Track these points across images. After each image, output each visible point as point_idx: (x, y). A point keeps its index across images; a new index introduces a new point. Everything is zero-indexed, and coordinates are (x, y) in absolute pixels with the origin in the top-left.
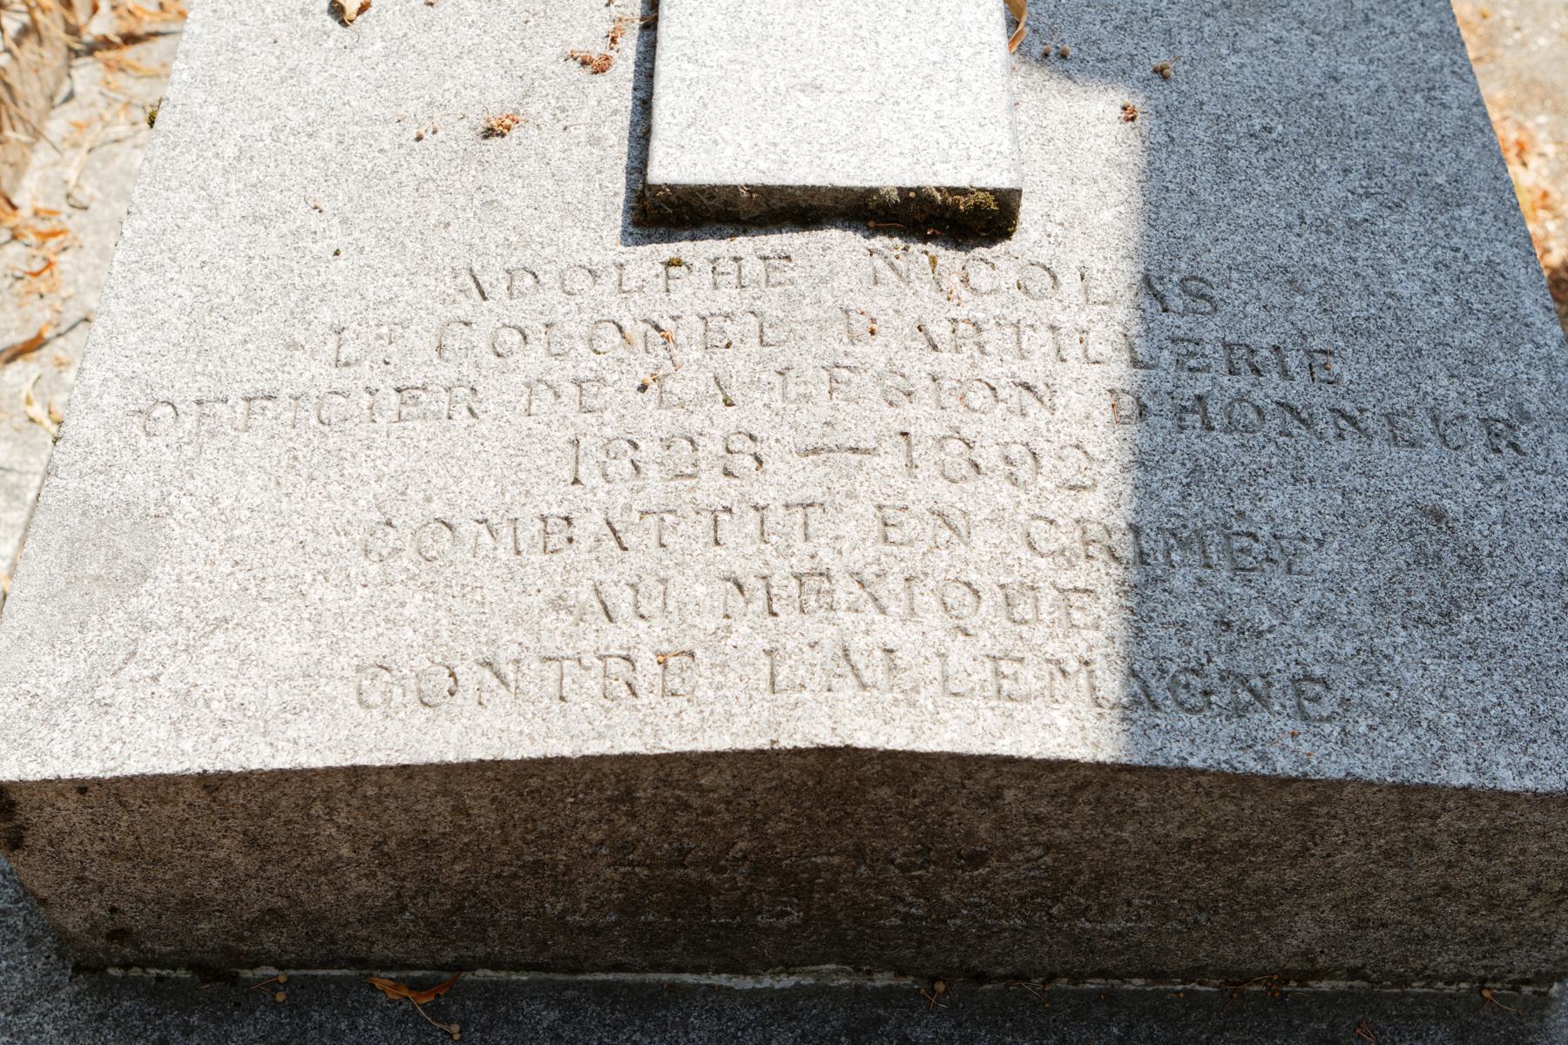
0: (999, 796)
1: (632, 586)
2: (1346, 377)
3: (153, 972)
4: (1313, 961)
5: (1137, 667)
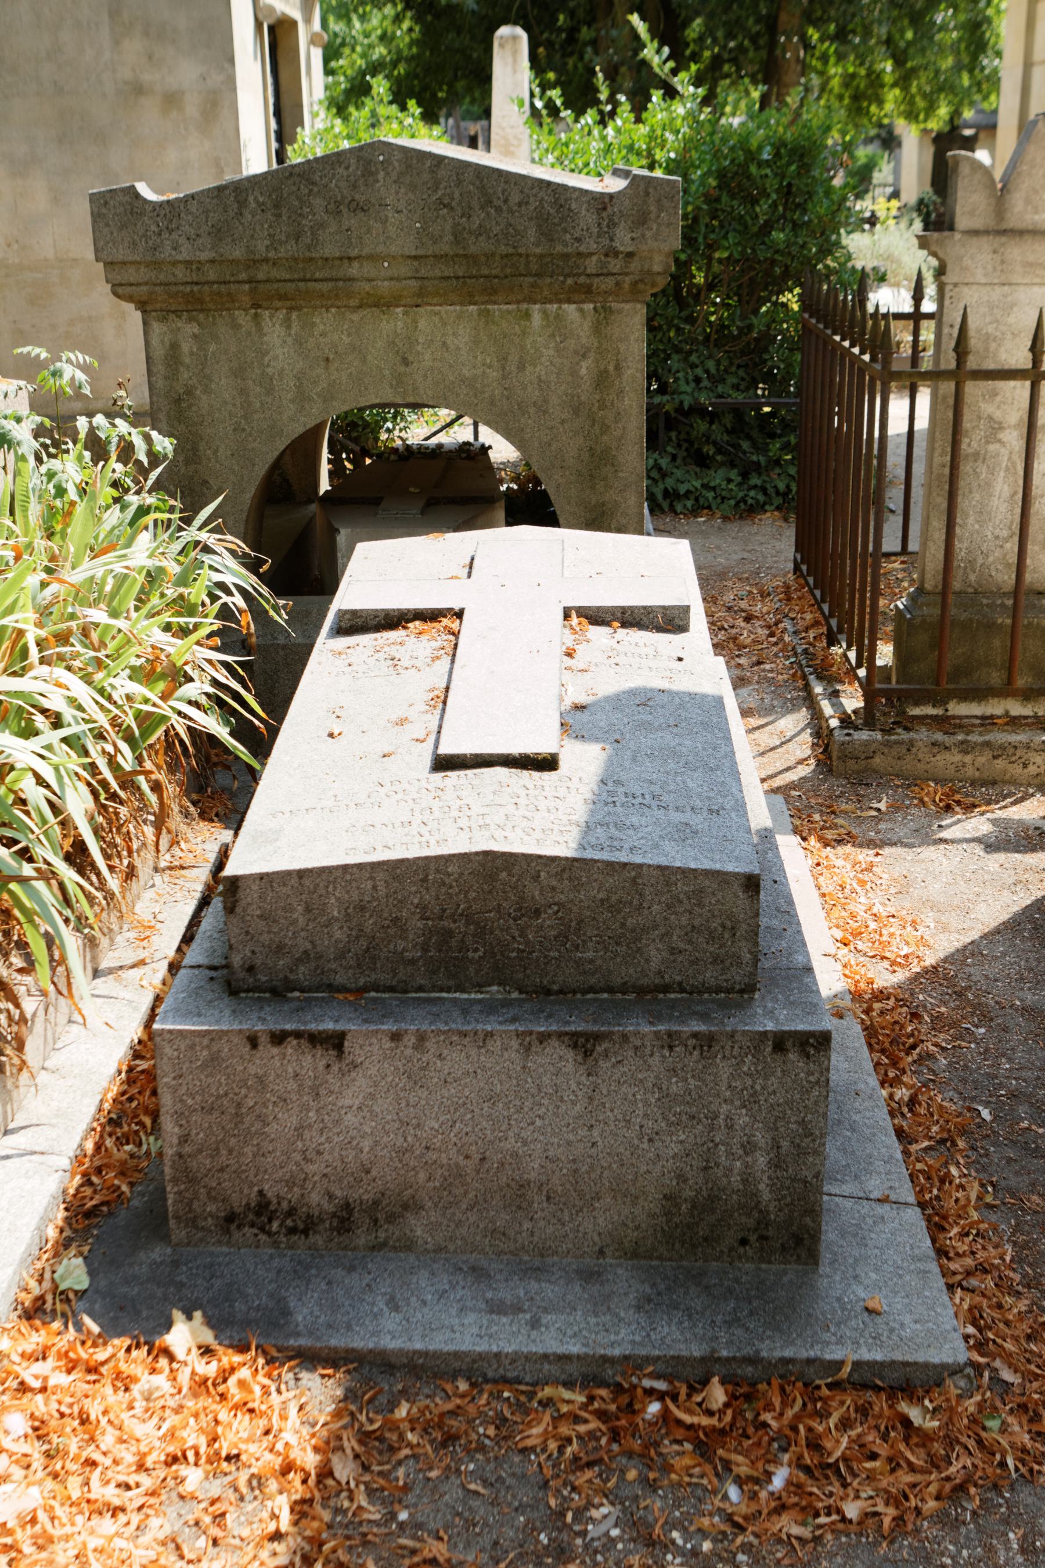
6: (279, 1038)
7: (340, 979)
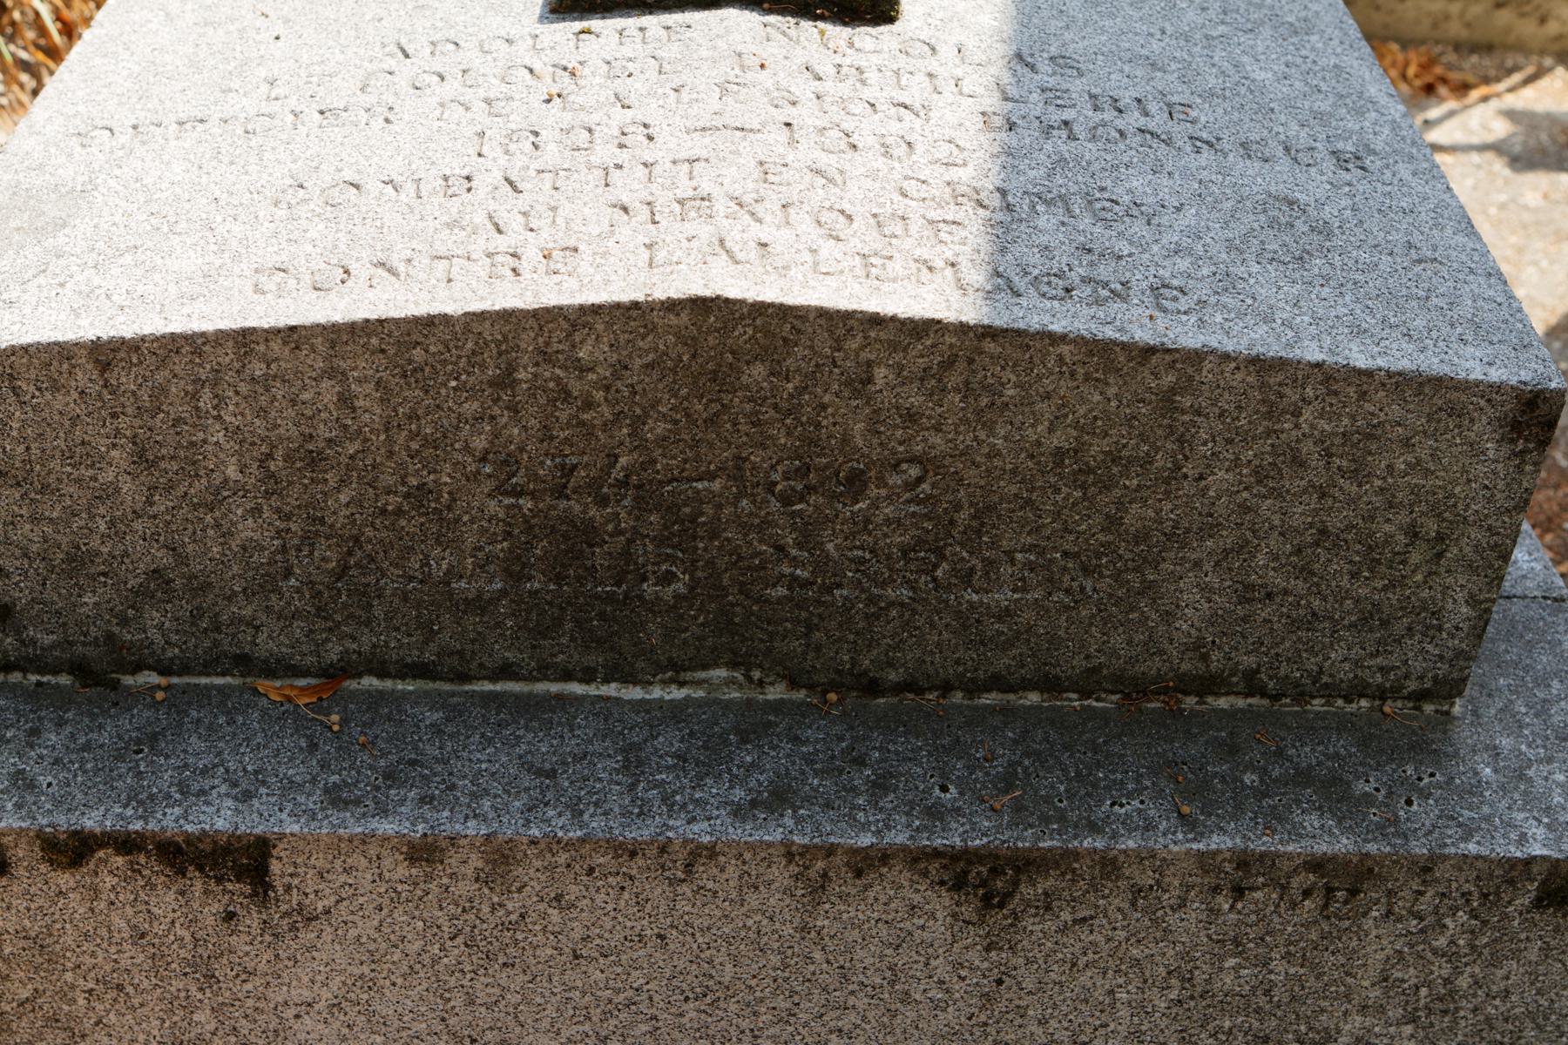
0: (870, 380)
1: (524, 214)
2: (1203, 119)
3: (33, 678)
4: (1205, 658)
5: (1001, 269)
6: (72, 850)
7: (267, 644)
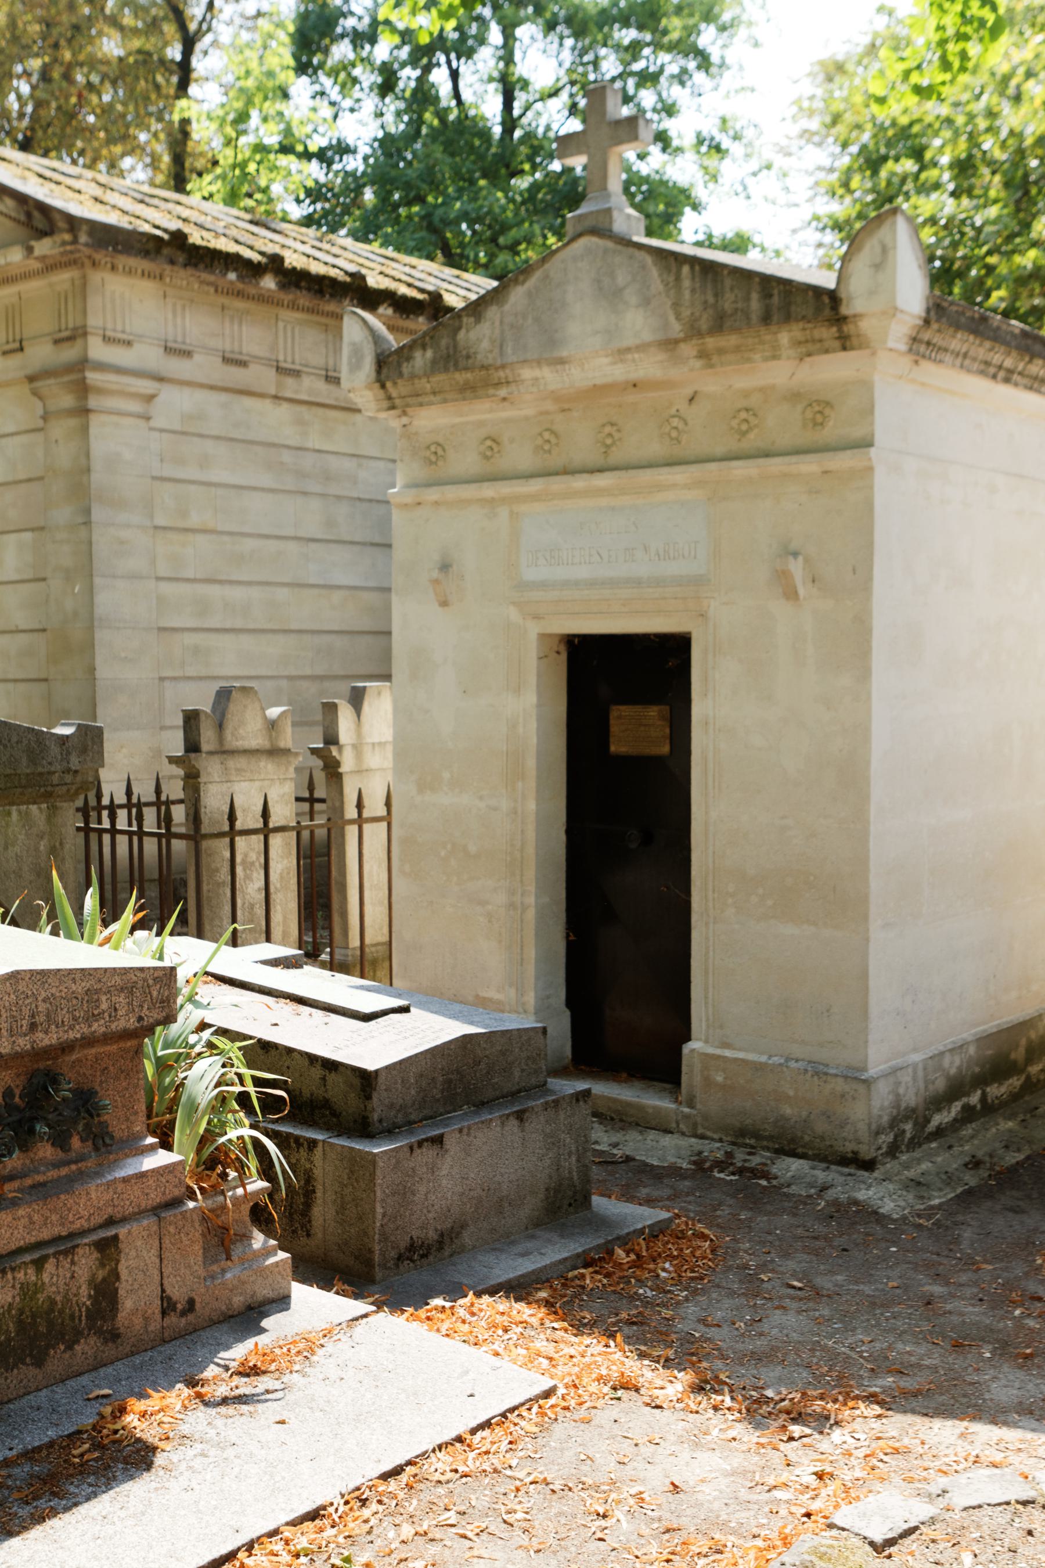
6: (420, 1144)
